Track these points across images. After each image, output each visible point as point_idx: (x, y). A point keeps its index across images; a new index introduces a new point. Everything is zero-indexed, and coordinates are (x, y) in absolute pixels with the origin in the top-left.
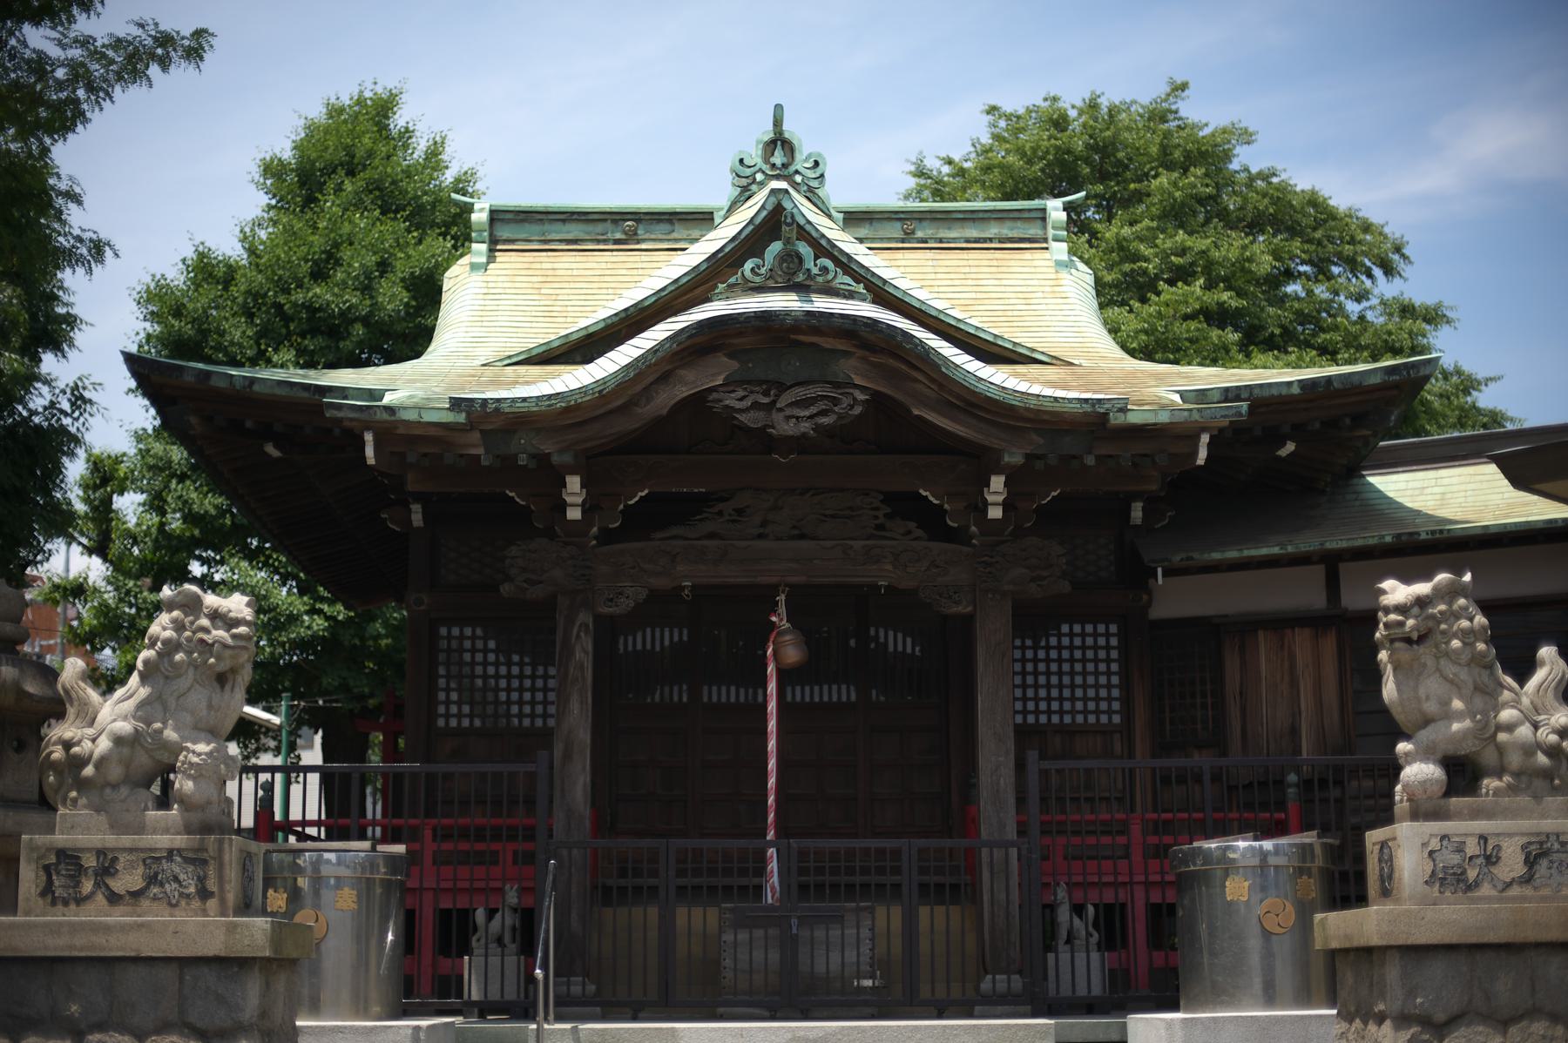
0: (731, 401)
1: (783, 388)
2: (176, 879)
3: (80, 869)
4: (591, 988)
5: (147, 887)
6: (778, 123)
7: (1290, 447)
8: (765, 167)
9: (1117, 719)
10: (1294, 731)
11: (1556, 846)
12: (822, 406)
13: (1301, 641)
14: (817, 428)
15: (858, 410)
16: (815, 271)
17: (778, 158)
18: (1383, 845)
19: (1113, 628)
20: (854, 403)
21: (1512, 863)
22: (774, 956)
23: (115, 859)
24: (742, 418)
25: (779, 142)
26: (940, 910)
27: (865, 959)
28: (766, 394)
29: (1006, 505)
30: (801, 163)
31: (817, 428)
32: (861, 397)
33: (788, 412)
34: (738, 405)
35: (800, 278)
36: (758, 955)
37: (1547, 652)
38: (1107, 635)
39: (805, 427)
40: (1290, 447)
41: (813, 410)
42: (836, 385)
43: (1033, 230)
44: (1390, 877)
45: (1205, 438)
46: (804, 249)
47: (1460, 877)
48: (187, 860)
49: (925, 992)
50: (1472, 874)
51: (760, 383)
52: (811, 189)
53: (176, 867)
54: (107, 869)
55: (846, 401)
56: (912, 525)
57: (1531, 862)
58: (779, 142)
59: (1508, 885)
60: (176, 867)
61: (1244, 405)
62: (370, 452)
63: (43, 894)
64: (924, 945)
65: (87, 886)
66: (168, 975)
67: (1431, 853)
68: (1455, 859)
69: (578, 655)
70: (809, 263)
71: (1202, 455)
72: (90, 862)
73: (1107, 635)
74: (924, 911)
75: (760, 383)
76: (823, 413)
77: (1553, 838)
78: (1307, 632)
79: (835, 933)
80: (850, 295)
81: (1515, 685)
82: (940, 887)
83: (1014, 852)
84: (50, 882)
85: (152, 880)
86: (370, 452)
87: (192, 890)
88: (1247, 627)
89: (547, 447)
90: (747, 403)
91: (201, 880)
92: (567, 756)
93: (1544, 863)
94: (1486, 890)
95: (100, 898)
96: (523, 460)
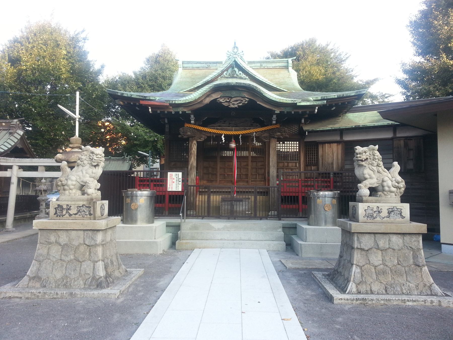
0: (221, 100)
1: (232, 98)
2: (84, 211)
3: (63, 209)
4: (195, 213)
5: (78, 213)
6: (235, 43)
7: (334, 108)
8: (233, 53)
9: (297, 150)
10: (332, 163)
11: (396, 210)
12: (239, 102)
13: (334, 146)
14: (239, 106)
15: (246, 103)
16: (238, 74)
17: (235, 50)
18: (354, 206)
19: (297, 143)
20: (245, 101)
21: (385, 213)
22: (229, 207)
23: (71, 206)
24: (224, 104)
25: (235, 47)
26: (261, 197)
27: (247, 208)
28: (228, 99)
29: (276, 121)
30: (240, 51)
31: (239, 106)
32: (247, 100)
33: (233, 103)
34: (223, 101)
35: (235, 76)
36: (226, 207)
37: (396, 163)
38: (296, 144)
39: (236, 106)
40: (334, 108)
41: (238, 102)
42: (242, 97)
43: (185, 65)
44: (355, 214)
45: (317, 108)
46: (236, 69)
47: (372, 216)
48: (86, 207)
49: (258, 215)
50: (375, 215)
51: (227, 97)
52: (241, 57)
53: (84, 209)
54: (69, 209)
55: (244, 101)
56: (258, 124)
57: (389, 213)
58: (235, 47)
59: (384, 218)
60: (84, 209)
61: (325, 101)
62: (150, 110)
63: (55, 214)
64: (258, 204)
65: (64, 212)
66: (82, 232)
67: (365, 210)
68: (371, 212)
69: (194, 149)
70: (237, 73)
71: (316, 111)
72: (65, 207)
73: (296, 144)
74: (258, 197)
75: (227, 97)
76: (240, 103)
77: (395, 208)
78: (336, 144)
79: (241, 203)
80: (245, 79)
81: (387, 171)
82: (261, 192)
83: (276, 189)
84: (56, 211)
85: (79, 211)
86: (150, 110)
87: (88, 213)
88: (324, 143)
89: (185, 110)
90: (225, 101)
91: (90, 211)
92: (191, 169)
93: (393, 213)
94: (378, 219)
95: (67, 215)
96: (180, 112)
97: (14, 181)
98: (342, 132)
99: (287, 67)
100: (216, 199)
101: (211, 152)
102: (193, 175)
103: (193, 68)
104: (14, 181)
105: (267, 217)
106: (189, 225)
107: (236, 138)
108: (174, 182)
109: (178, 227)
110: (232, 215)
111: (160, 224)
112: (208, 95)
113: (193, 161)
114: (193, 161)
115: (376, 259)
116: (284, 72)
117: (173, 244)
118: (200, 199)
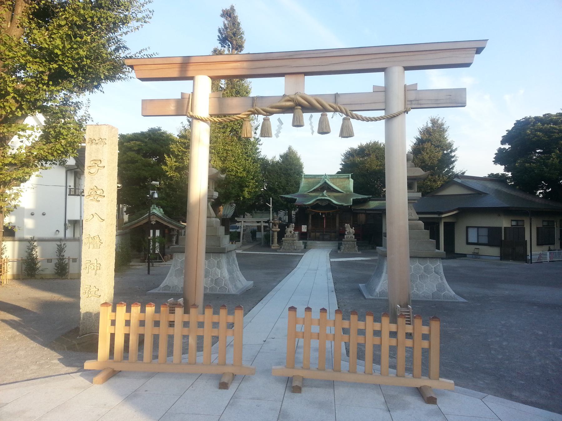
97: (262, 227)
98: (366, 210)
99: (349, 178)
100: (318, 234)
101: (316, 217)
102: (310, 226)
103: (308, 178)
104: (262, 227)
105: (335, 240)
106: (309, 242)
107: (325, 213)
108: (304, 228)
109: (306, 243)
110: (323, 240)
111: (301, 242)
112: (315, 202)
113: (310, 221)
114: (310, 221)
115: (347, 246)
116: (347, 181)
117: (305, 248)
118: (313, 234)
